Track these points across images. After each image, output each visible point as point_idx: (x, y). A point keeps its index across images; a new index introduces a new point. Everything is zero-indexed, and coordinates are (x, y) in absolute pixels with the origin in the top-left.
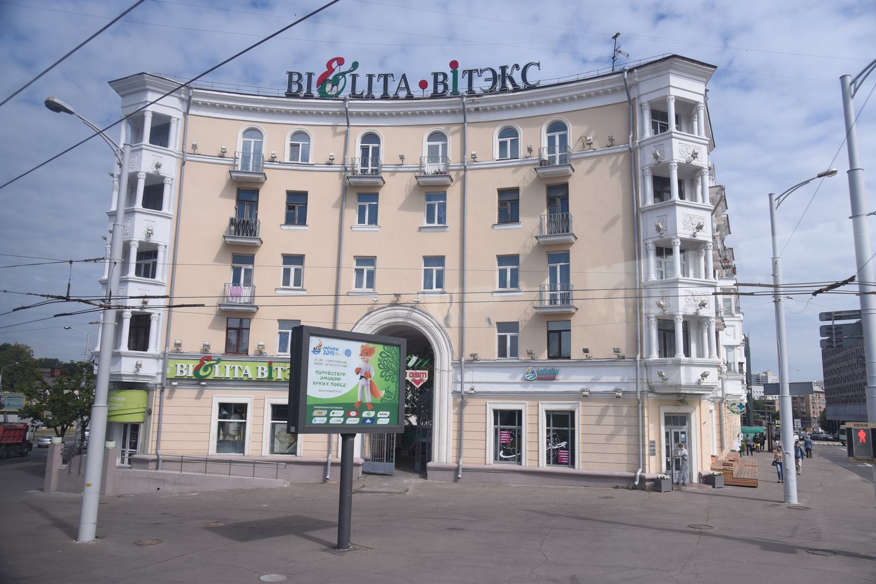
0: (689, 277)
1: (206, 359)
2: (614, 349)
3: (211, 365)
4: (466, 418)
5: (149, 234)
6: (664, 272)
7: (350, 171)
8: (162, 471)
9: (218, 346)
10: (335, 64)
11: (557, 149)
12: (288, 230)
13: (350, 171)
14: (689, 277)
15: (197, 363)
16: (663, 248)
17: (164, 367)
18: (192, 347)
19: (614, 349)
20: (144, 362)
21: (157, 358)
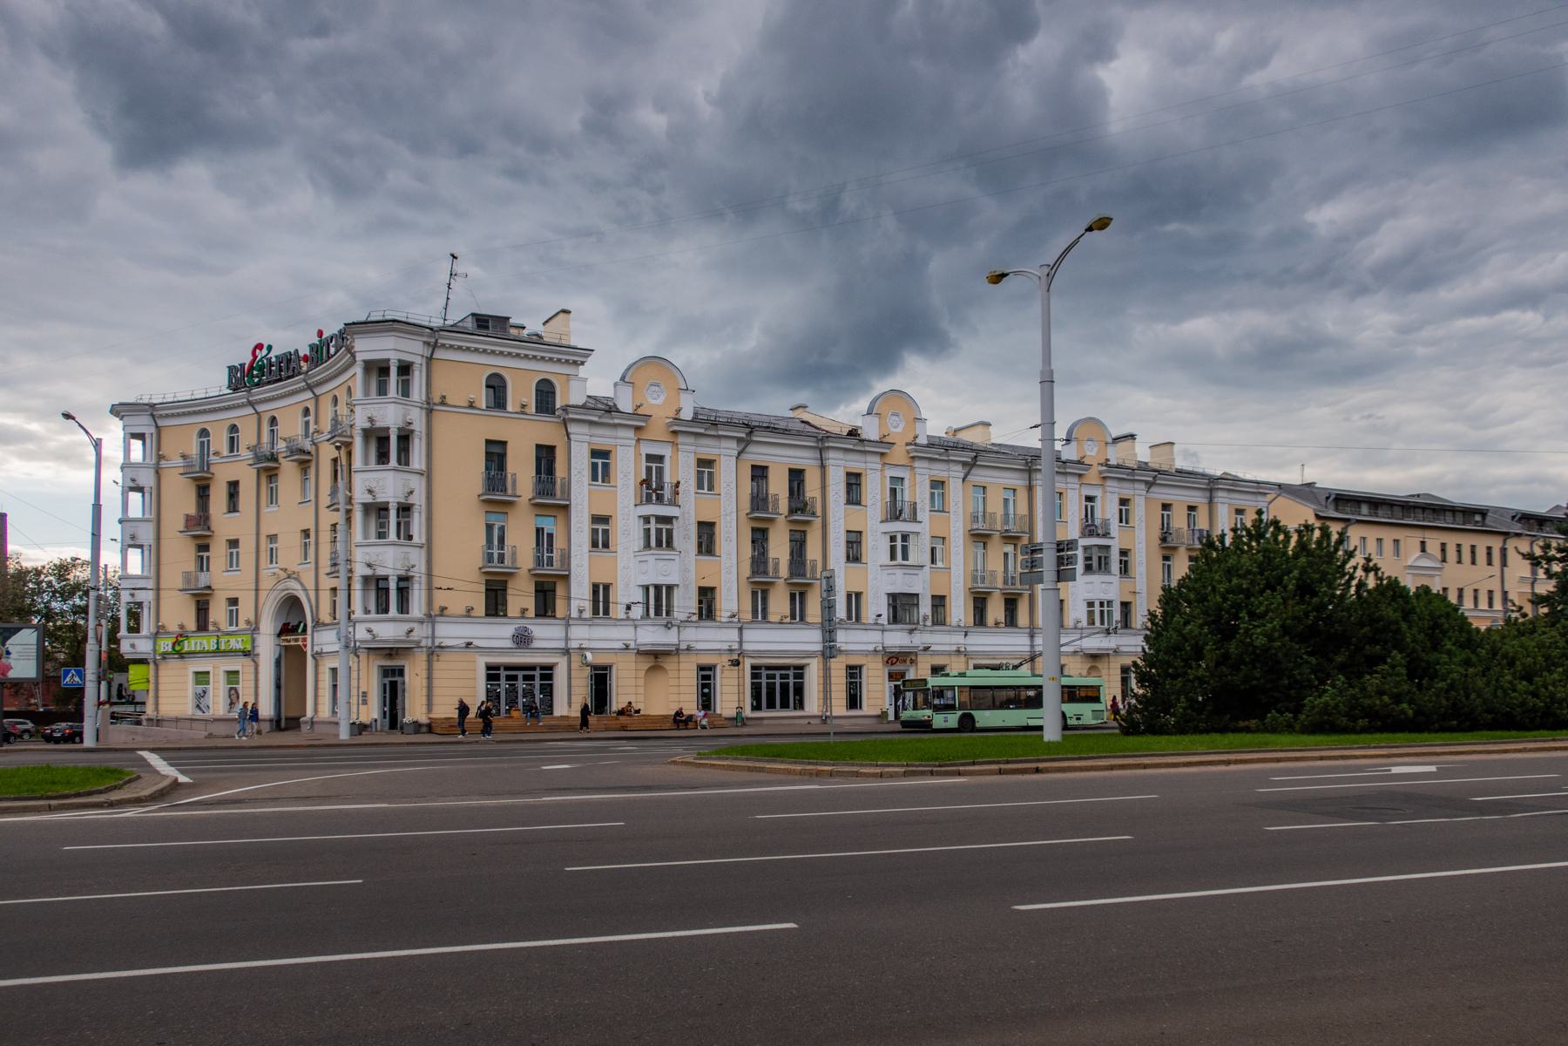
0: (908, 560)
1: (181, 636)
2: (636, 505)
3: (182, 641)
4: (436, 674)
5: (1223, 531)
6: (274, 489)
7: (1382, 701)
8: (693, 499)
9: (191, 625)
10: (258, 351)
11: (764, 685)
12: (231, 517)
13: (1382, 701)
14: (908, 560)
15: (174, 640)
16: (552, 680)
17: (155, 644)
18: (173, 627)
19: (636, 505)
20: (137, 642)
21: (146, 637)
